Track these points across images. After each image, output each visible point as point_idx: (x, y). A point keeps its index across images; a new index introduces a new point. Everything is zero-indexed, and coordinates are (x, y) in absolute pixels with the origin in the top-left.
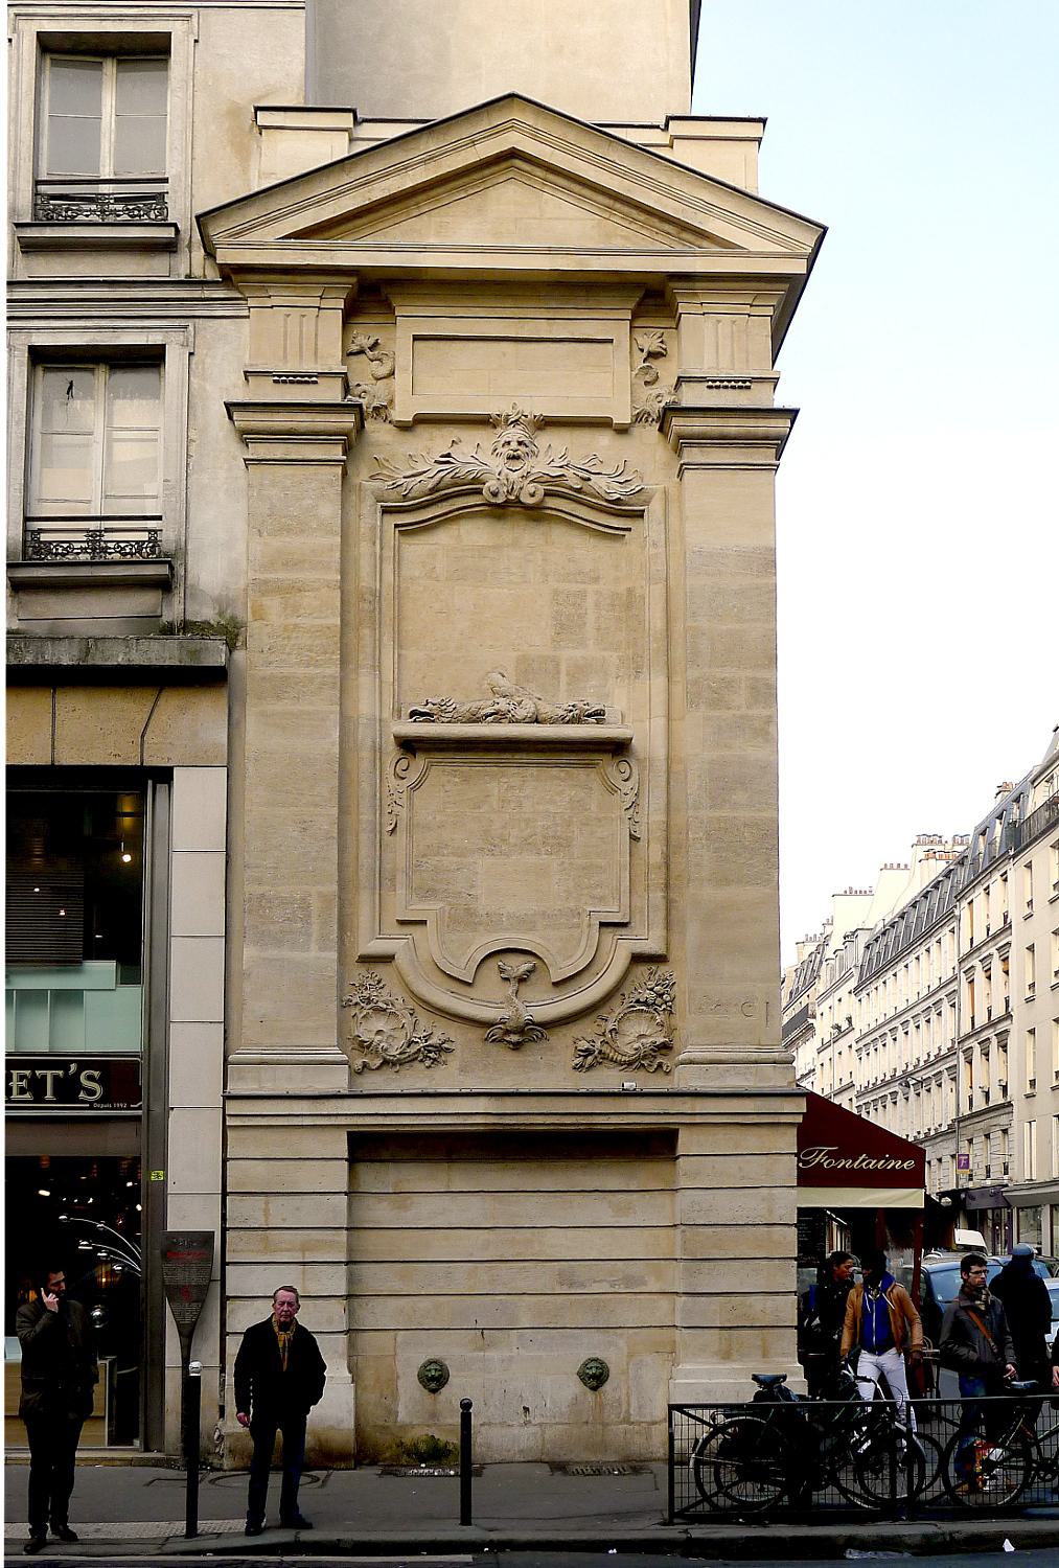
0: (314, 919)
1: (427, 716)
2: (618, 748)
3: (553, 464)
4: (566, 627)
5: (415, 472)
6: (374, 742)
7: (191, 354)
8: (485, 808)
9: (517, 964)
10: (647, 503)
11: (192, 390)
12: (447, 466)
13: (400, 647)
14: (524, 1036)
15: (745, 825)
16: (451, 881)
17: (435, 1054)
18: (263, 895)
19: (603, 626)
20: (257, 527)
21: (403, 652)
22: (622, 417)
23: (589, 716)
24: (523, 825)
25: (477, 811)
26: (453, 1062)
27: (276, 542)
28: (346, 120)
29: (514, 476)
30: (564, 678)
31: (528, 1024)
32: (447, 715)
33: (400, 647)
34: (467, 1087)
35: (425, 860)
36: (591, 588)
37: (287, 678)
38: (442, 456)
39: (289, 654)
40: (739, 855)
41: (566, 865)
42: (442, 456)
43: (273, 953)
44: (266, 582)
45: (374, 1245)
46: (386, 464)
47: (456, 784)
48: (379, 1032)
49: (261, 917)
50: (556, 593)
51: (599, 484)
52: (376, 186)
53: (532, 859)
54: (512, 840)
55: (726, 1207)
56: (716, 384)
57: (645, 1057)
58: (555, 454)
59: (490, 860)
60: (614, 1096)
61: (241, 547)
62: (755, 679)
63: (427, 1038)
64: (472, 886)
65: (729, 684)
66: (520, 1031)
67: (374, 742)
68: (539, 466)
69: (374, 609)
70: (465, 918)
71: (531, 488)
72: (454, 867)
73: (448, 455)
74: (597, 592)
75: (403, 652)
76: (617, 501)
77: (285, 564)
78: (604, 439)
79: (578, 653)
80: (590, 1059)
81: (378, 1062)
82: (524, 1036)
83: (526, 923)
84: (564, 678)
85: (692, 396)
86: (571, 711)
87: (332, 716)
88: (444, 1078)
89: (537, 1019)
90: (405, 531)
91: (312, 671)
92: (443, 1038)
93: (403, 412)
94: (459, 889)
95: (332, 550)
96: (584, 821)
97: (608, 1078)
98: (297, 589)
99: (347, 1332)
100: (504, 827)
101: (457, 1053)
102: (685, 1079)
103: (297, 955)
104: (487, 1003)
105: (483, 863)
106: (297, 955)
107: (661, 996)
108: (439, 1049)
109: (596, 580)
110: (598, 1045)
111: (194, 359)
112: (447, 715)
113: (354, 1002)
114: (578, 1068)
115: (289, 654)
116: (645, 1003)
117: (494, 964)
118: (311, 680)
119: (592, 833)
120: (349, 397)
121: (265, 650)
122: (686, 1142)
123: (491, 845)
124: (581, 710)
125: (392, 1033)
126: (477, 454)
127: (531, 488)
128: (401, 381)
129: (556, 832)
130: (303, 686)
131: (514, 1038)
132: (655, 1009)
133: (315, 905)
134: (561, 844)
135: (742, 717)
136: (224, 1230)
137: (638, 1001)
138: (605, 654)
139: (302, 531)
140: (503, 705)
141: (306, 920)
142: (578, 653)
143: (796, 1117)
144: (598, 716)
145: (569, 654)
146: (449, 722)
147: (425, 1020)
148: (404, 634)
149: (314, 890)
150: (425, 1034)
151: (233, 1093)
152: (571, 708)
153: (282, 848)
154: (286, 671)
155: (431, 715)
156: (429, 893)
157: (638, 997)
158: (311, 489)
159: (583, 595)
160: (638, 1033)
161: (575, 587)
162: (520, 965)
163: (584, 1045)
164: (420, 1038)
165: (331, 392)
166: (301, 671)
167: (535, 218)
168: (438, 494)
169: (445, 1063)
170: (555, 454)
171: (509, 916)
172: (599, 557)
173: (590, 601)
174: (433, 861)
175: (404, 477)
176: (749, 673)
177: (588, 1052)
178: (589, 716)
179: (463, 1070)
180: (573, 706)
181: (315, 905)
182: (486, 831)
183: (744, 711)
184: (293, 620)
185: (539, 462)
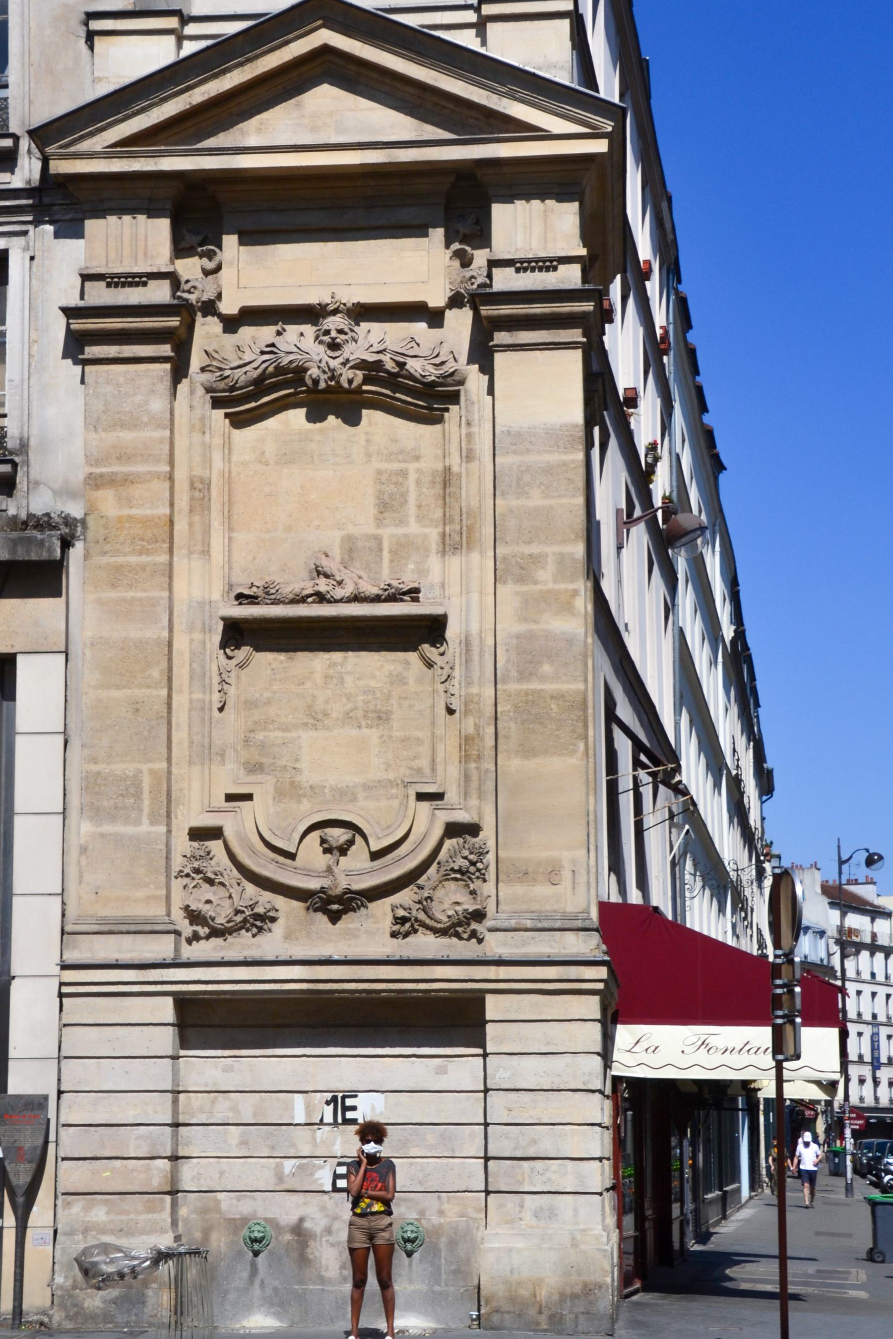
0: (146, 795)
1: (252, 600)
2: (432, 629)
3: (372, 349)
4: (388, 506)
5: (242, 362)
6: (204, 624)
7: (32, 258)
8: (308, 685)
9: (339, 834)
10: (462, 383)
11: (33, 291)
12: (272, 356)
13: (231, 529)
14: (335, 905)
15: (552, 697)
16: (277, 756)
17: (259, 922)
18: (98, 773)
19: (424, 503)
20: (93, 423)
21: (234, 535)
22: (437, 299)
23: (404, 594)
24: (344, 700)
25: (301, 687)
26: (278, 929)
27: (111, 437)
28: (172, 22)
29: (334, 364)
30: (386, 555)
31: (345, 893)
32: (271, 597)
33: (231, 529)
34: (293, 953)
35: (252, 735)
36: (412, 467)
37: (121, 566)
38: (267, 346)
39: (123, 544)
40: (546, 727)
41: (385, 738)
42: (267, 346)
43: (107, 828)
44: (101, 476)
45: (193, 1107)
46: (215, 355)
47: (281, 662)
48: (208, 902)
49: (97, 794)
50: (379, 472)
51: (415, 366)
52: (197, 91)
53: (354, 732)
54: (334, 715)
55: (530, 1072)
56: (522, 265)
57: (459, 924)
58: (375, 339)
59: (312, 733)
60: (435, 966)
61: (79, 442)
62: (561, 554)
63: (252, 907)
64: (297, 760)
65: (537, 560)
66: (339, 899)
67: (204, 624)
68: (355, 351)
69: (204, 497)
70: (289, 791)
71: (350, 374)
72: (280, 741)
73: (273, 345)
74: (418, 470)
75: (234, 535)
76: (433, 384)
77: (119, 458)
78: (420, 328)
79: (400, 531)
80: (404, 926)
81: (207, 930)
82: (335, 905)
83: (345, 794)
84: (386, 555)
85: (505, 280)
86: (386, 590)
87: (162, 602)
88: (270, 944)
89: (356, 887)
90: (239, 421)
91: (144, 559)
92: (268, 906)
93: (228, 307)
94: (284, 763)
95: (161, 443)
96: (403, 695)
97: (425, 944)
98: (127, 480)
99: (178, 1192)
100: (327, 702)
101: (281, 922)
102: (496, 945)
103: (129, 830)
104: (308, 873)
105: (306, 737)
106: (129, 830)
107: (473, 864)
108: (262, 917)
109: (417, 458)
110: (414, 913)
111: (35, 262)
112: (271, 597)
113: (185, 872)
114: (394, 935)
115: (123, 544)
116: (460, 871)
117: (315, 835)
118: (143, 568)
119: (411, 706)
120: (179, 294)
121: (101, 540)
122: (493, 1007)
123: (315, 719)
124: (397, 589)
125: (220, 902)
126: (299, 342)
127: (350, 374)
128: (226, 275)
129: (376, 705)
130: (136, 574)
131: (335, 907)
132: (470, 878)
133: (146, 782)
134: (382, 718)
135: (548, 591)
136: (60, 1093)
137: (452, 870)
138: (426, 530)
139: (135, 426)
140: (323, 585)
141: (138, 795)
142: (400, 531)
143: (598, 984)
144: (413, 594)
145: (388, 533)
146: (272, 604)
147: (251, 889)
148: (235, 517)
149: (145, 767)
150: (251, 903)
151: (68, 962)
152: (386, 587)
153: (116, 728)
154: (120, 560)
155: (256, 598)
156: (255, 768)
157: (452, 865)
158: (140, 383)
159: (404, 474)
160: (450, 900)
161: (396, 466)
162: (338, 835)
163: (401, 913)
164: (246, 907)
165: (158, 293)
166: (133, 559)
167: (351, 110)
168: (260, 385)
169: (270, 930)
170: (375, 339)
171: (332, 789)
172: (420, 436)
173: (412, 477)
174: (260, 736)
175: (232, 369)
176: (556, 549)
177: (403, 920)
178: (404, 594)
179: (288, 937)
180: (389, 585)
181: (146, 782)
182: (309, 707)
183: (551, 586)
184: (126, 512)
185: (358, 348)
